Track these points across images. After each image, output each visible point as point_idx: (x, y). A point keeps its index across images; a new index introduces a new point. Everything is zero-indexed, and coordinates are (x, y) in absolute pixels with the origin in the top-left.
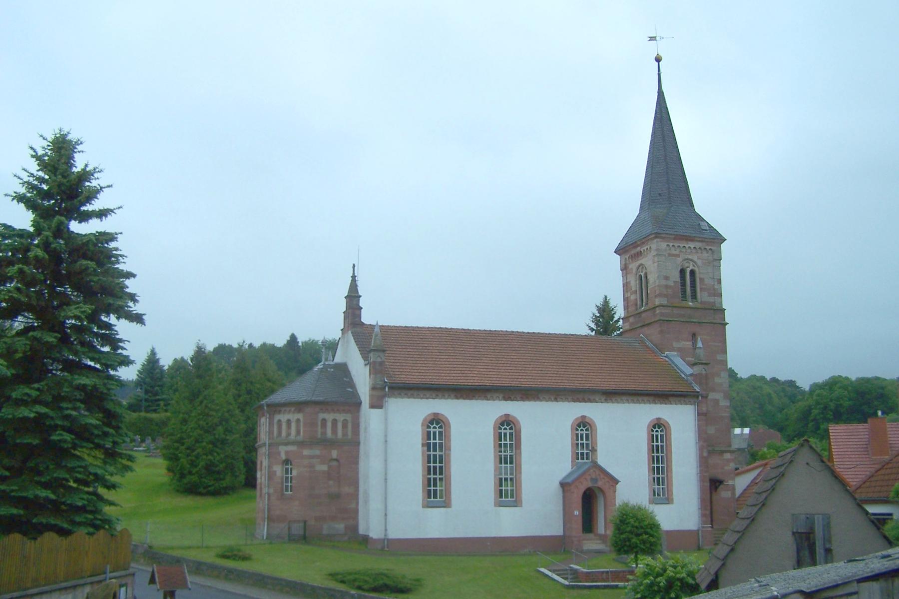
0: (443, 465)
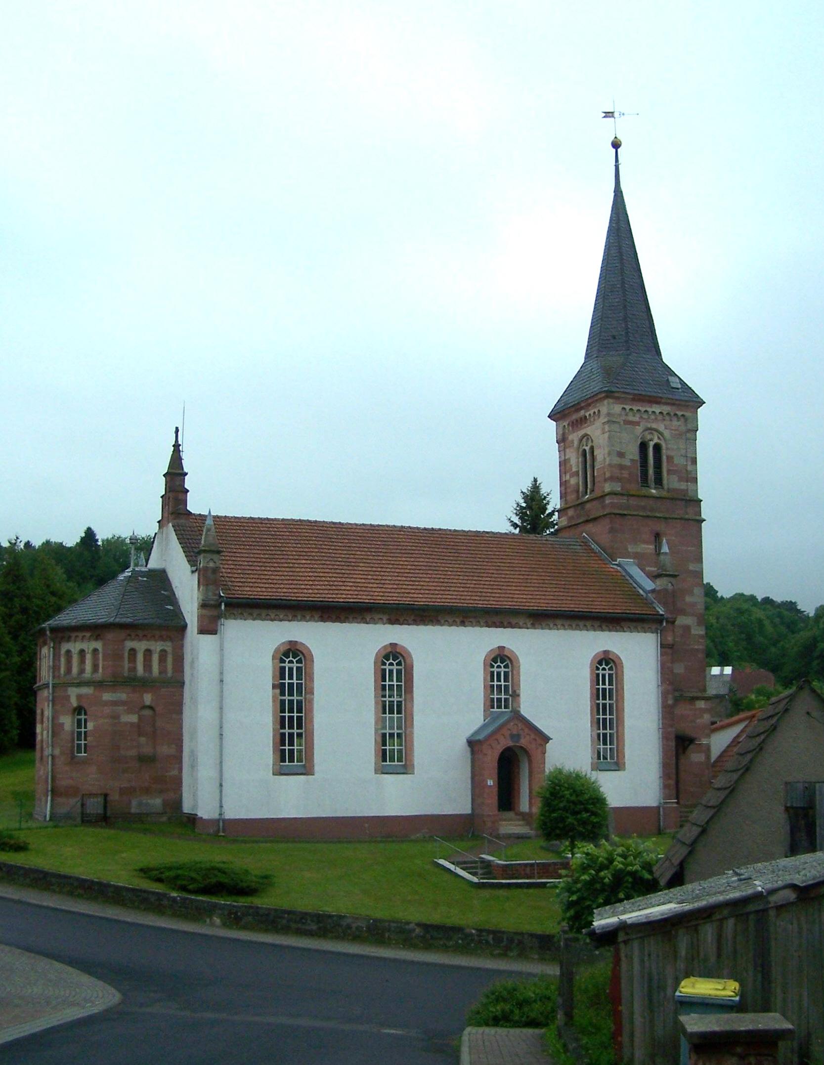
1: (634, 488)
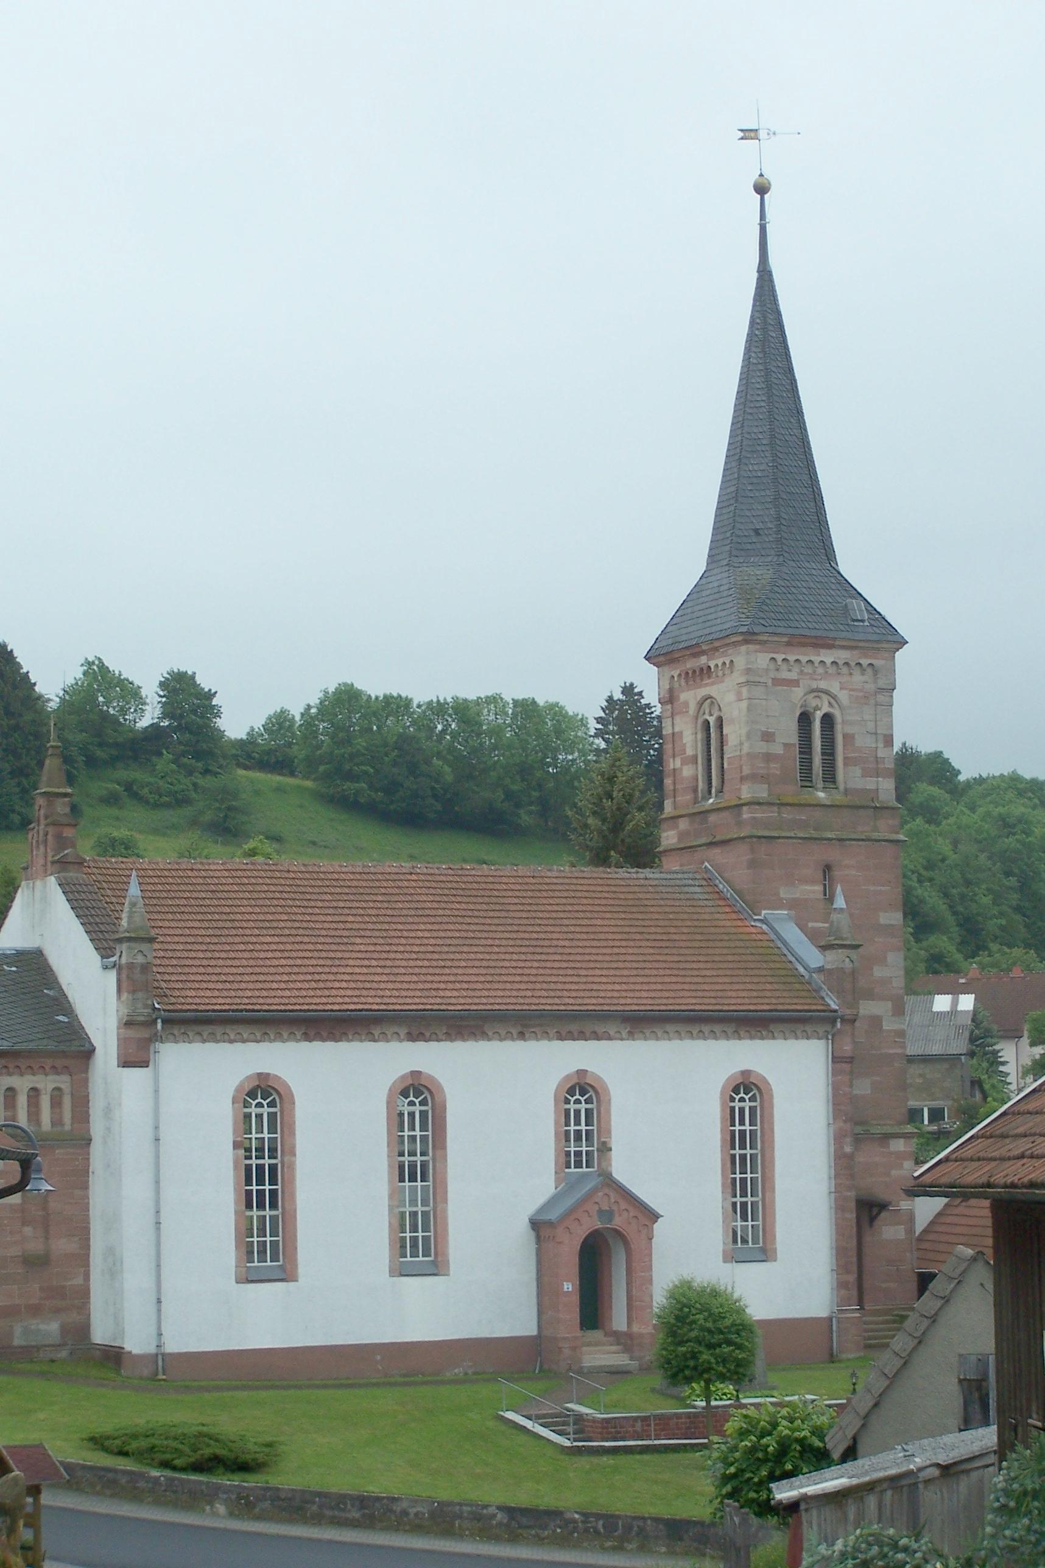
0: (279, 1187)
1: (790, 791)
